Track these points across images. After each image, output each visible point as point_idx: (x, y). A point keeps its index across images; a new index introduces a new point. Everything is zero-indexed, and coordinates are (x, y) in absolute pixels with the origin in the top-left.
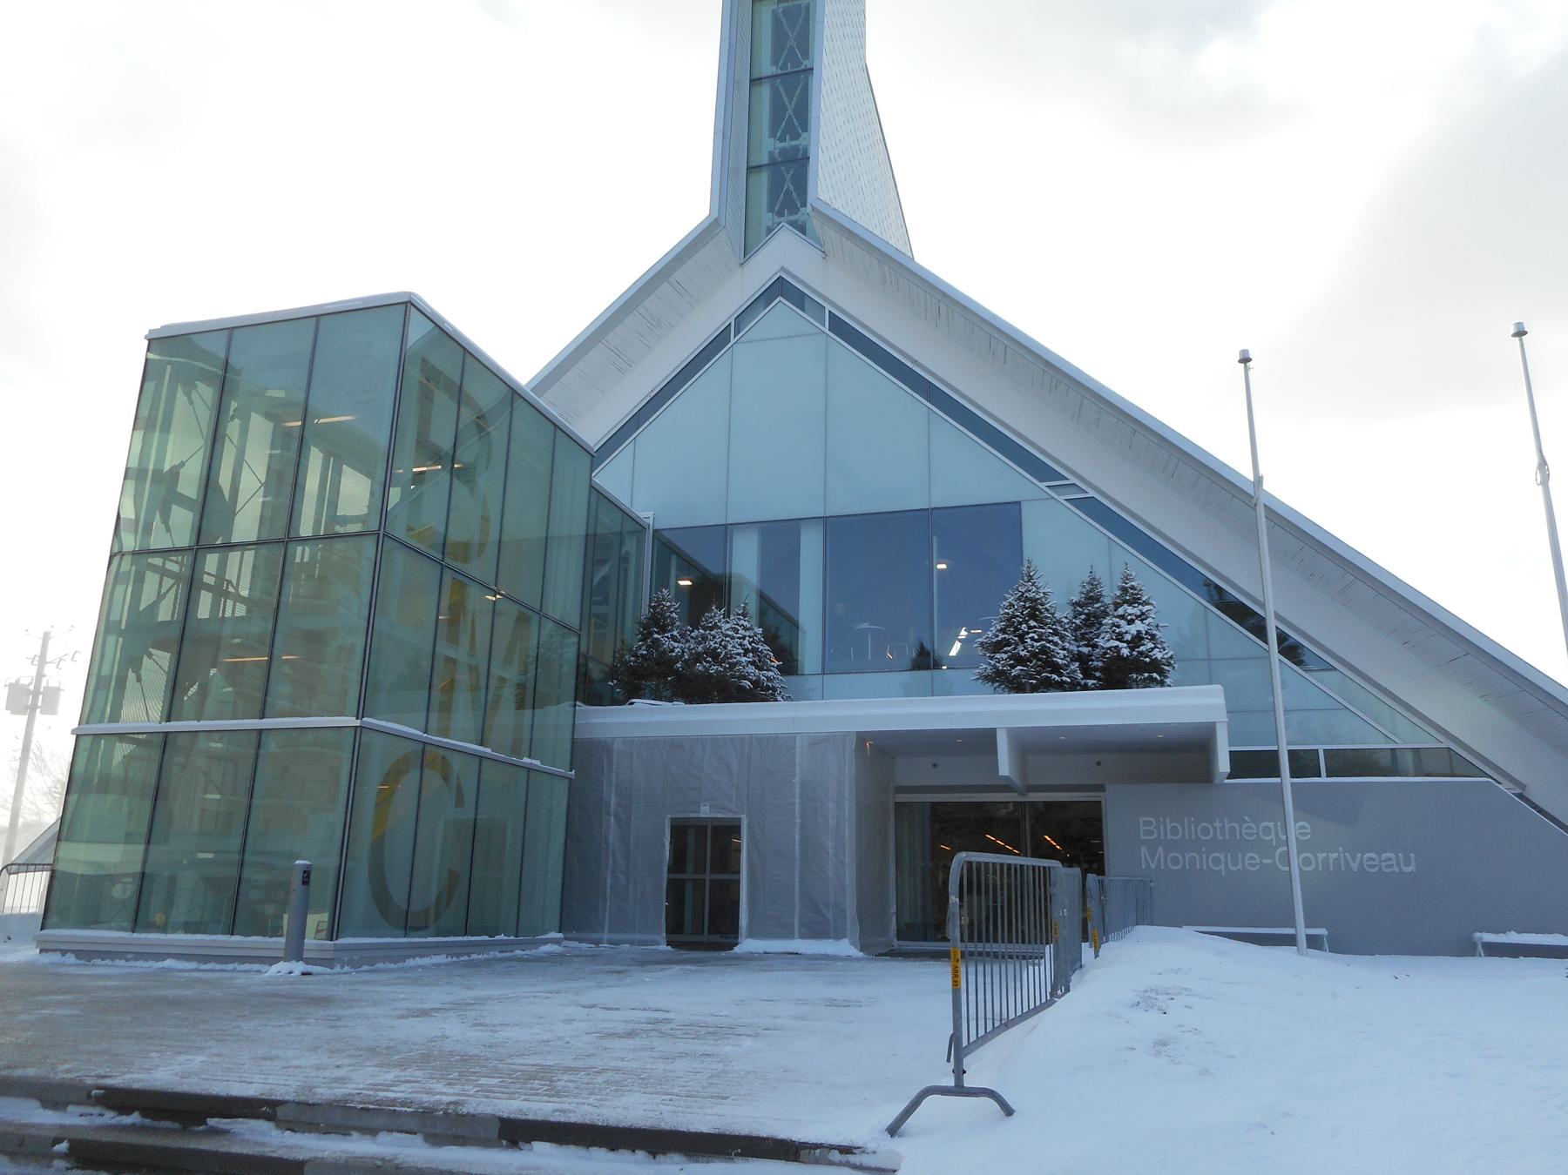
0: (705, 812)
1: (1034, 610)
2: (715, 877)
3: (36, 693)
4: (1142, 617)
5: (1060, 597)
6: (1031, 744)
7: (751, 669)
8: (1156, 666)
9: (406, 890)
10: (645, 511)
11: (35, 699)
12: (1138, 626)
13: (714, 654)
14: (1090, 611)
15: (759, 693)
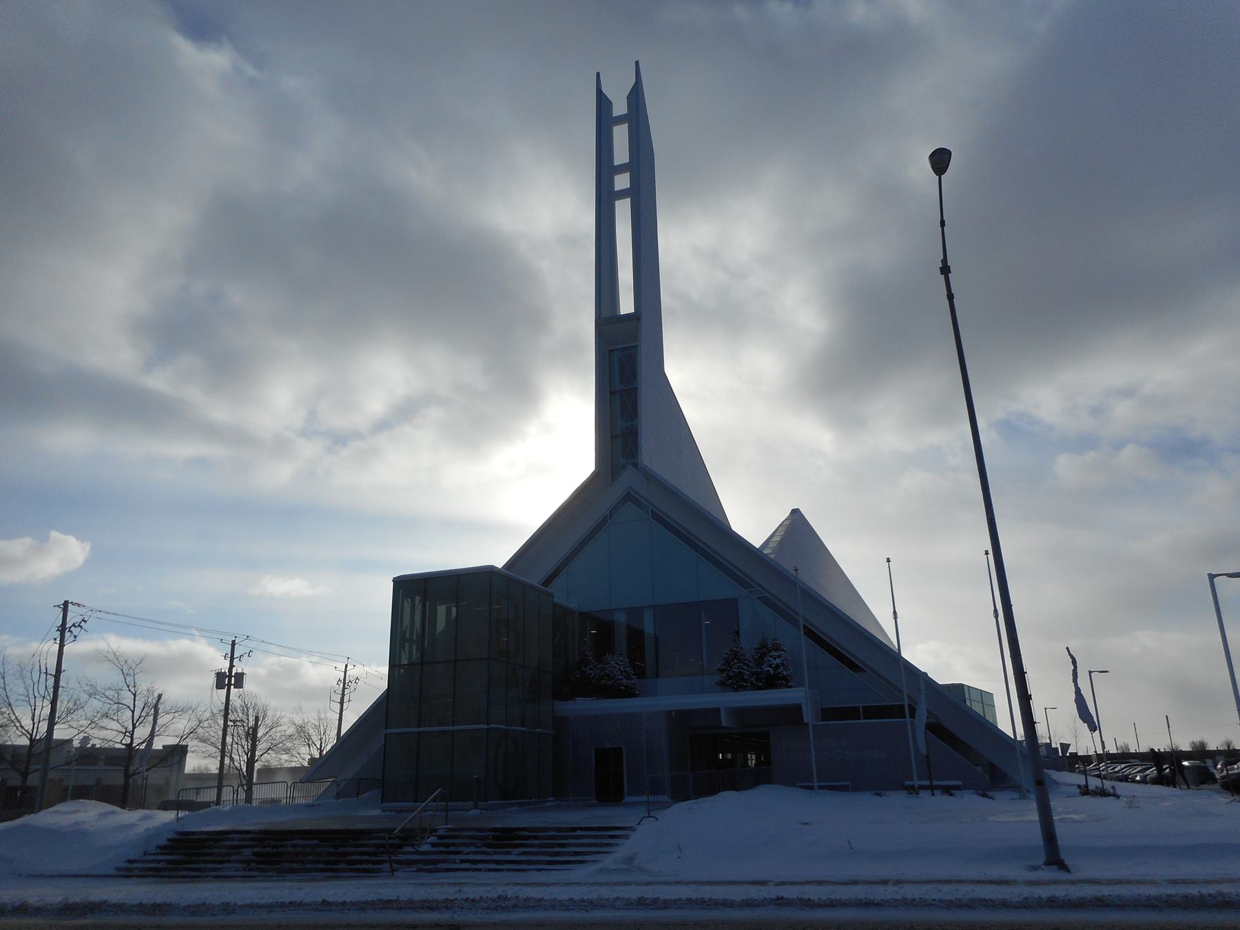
0: (608, 745)
1: (736, 655)
2: (915, 777)
3: (230, 677)
4: (779, 657)
5: (748, 645)
6: (741, 713)
7: (624, 681)
8: (784, 678)
9: (984, 597)
10: (572, 605)
11: (230, 681)
12: (778, 661)
13: (608, 676)
14: (764, 650)
15: (629, 693)
